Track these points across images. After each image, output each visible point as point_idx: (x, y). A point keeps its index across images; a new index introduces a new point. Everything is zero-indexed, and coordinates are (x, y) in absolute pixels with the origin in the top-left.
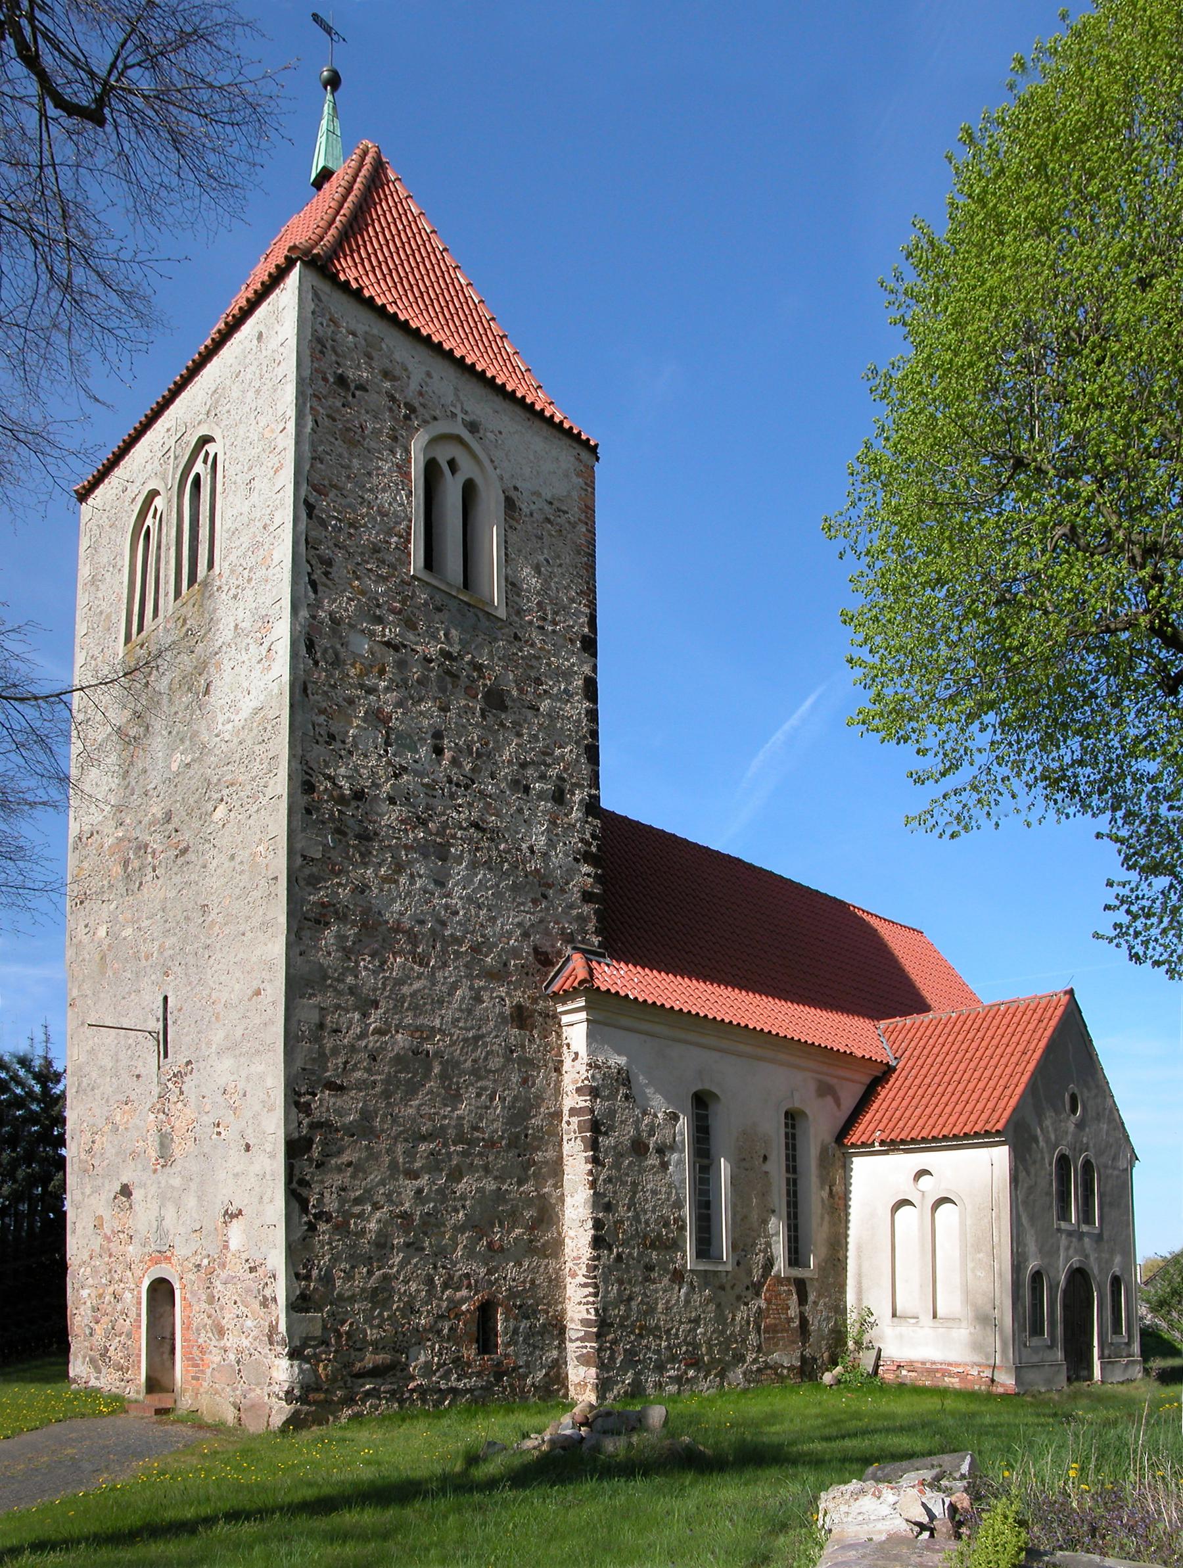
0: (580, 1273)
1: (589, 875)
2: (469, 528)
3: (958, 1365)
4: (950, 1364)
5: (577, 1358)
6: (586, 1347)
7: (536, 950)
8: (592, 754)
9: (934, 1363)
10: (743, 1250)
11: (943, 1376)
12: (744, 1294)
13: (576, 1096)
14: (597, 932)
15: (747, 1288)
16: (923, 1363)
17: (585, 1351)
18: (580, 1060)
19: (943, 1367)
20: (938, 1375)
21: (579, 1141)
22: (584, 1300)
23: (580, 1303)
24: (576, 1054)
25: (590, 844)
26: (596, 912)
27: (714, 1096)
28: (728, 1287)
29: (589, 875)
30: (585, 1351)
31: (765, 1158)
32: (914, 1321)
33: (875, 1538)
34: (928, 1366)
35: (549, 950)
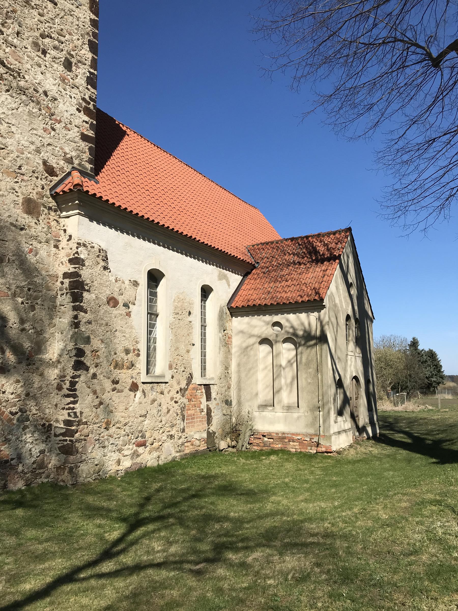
0: (65, 387)
1: (87, 122)
2: (234, 296)
3: (297, 434)
4: (293, 434)
5: (59, 448)
6: (66, 440)
7: (45, 163)
8: (267, 243)
9: (284, 433)
10: (175, 369)
11: (289, 441)
12: (175, 396)
13: (68, 265)
14: (90, 162)
15: (177, 392)
16: (277, 434)
17: (65, 443)
18: (72, 240)
19: (289, 436)
20: (286, 441)
21: (69, 296)
22: (67, 407)
23: (63, 409)
24: (70, 236)
25: (89, 103)
26: (90, 149)
27: (162, 275)
28: (165, 392)
29: (87, 122)
30: (65, 443)
31: (190, 313)
32: (271, 408)
33: (171, 338)
34: (280, 435)
35: (55, 165)
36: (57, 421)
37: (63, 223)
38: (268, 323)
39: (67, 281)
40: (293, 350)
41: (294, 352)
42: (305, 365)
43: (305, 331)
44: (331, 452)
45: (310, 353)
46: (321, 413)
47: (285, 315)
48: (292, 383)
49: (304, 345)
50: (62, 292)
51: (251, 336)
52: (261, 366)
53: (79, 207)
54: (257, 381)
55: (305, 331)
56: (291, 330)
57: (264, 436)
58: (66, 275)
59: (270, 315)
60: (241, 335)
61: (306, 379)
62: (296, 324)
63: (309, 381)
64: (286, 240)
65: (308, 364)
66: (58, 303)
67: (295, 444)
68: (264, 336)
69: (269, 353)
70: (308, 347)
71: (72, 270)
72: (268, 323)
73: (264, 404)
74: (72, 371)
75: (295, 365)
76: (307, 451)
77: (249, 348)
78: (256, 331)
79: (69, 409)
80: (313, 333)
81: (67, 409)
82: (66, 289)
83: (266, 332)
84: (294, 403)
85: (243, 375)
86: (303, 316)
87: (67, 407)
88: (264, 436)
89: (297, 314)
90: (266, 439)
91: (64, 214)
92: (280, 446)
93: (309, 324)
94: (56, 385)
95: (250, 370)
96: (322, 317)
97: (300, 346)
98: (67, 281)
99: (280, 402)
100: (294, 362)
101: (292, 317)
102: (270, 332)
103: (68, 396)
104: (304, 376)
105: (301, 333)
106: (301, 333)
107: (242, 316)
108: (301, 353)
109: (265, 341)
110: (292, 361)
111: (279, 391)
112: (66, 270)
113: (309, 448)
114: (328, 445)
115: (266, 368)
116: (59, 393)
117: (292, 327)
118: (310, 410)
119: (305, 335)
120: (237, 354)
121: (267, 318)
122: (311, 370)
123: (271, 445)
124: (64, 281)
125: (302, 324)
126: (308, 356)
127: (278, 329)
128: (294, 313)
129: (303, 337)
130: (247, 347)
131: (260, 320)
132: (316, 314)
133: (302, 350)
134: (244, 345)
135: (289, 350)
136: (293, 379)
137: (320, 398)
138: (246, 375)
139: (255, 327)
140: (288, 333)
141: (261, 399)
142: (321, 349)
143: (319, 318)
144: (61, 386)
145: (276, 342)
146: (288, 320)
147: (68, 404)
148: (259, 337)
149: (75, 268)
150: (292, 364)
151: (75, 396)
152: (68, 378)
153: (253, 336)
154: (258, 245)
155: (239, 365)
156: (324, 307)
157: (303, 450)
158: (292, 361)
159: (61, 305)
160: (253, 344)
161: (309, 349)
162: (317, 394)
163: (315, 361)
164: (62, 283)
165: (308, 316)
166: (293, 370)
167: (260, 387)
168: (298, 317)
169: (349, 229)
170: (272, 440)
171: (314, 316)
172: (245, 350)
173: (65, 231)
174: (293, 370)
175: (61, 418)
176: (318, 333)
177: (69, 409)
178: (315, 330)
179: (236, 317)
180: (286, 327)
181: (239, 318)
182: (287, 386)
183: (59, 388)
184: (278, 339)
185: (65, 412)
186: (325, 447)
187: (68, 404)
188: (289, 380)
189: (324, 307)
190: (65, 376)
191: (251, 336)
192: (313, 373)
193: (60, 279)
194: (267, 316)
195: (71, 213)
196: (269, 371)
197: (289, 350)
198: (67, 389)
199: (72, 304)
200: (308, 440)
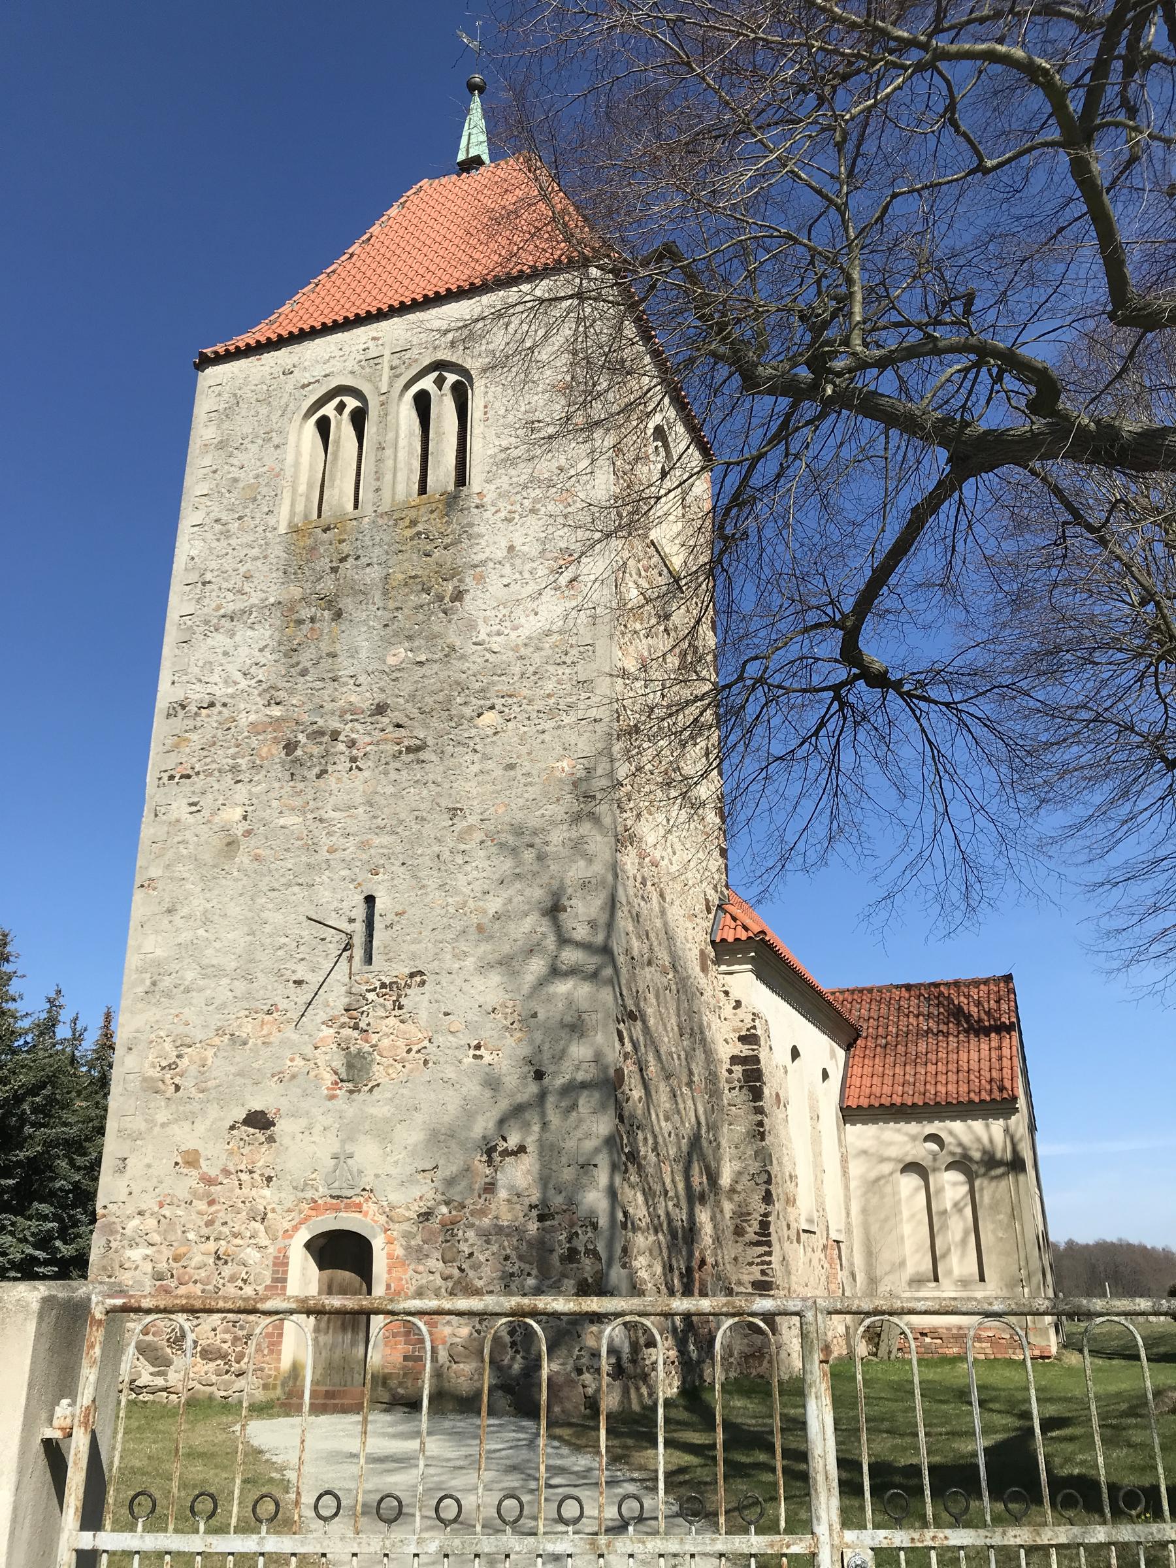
0: (749, 1229)
9: (960, 1328)
13: (739, 1044)
16: (947, 1329)
21: (744, 1091)
22: (759, 1260)
23: (751, 1264)
34: (954, 1331)
36: (740, 1283)
37: (723, 982)
38: (914, 1138)
39: (738, 1069)
40: (962, 1184)
41: (966, 1188)
42: (991, 1208)
43: (984, 1152)
44: (1049, 1357)
45: (997, 1187)
46: (1026, 1290)
47: (948, 1122)
48: (964, 1242)
49: (984, 1175)
50: (732, 1085)
51: (883, 1160)
52: (906, 1214)
53: (752, 961)
54: (902, 1238)
55: (984, 1152)
56: (959, 1150)
57: (923, 1334)
58: (734, 1060)
59: (919, 1121)
60: (863, 1158)
61: (994, 1232)
62: (966, 1139)
63: (1000, 1235)
64: (897, 987)
65: (995, 1207)
66: (726, 1102)
67: (984, 1345)
68: (909, 1159)
69: (917, 1189)
70: (993, 1178)
71: (751, 1053)
72: (914, 1138)
73: (918, 1278)
74: (764, 1206)
75: (968, 1211)
76: (1007, 1356)
77: (882, 1182)
78: (893, 1152)
79: (763, 1263)
80: (999, 1155)
81: (758, 1264)
82: (739, 1081)
83: (914, 1152)
84: (972, 1275)
85: (874, 1228)
86: (978, 1125)
87: (759, 1260)
88: (923, 1334)
89: (969, 1121)
90: (928, 1340)
91: (723, 968)
92: (955, 1350)
93: (991, 1141)
94: (732, 1228)
95: (886, 1220)
96: (1012, 1128)
97: (977, 1177)
98: (738, 1069)
99: (949, 1272)
100: (966, 1205)
101: (957, 1126)
102: (924, 1152)
103: (758, 1244)
104: (990, 1226)
105: (977, 1155)
106: (977, 1155)
107: (864, 1123)
108: (982, 1189)
109: (910, 1166)
110: (962, 1204)
111: (944, 1256)
112: (736, 1052)
113: (1010, 1351)
114: (1044, 1344)
115: (913, 1216)
116: (740, 1239)
117: (960, 1144)
118: (1006, 1285)
119: (986, 1158)
120: (859, 1193)
121: (913, 1128)
122: (1001, 1217)
123: (940, 1351)
124: (734, 1068)
125: (979, 1140)
126: (994, 1192)
127: (934, 1147)
128: (964, 1120)
129: (981, 1162)
130: (878, 1179)
131: (899, 1131)
132: (1001, 1122)
133: (981, 1184)
134: (873, 1175)
135: (955, 1184)
136: (966, 1233)
137: (1022, 1263)
138: (881, 1229)
139: (890, 1144)
140: (953, 1154)
141: (910, 1270)
142: (1017, 1181)
143: (1006, 1130)
144: (743, 1228)
145: (934, 1170)
146: (951, 1133)
147: (759, 1256)
148: (900, 1161)
149: (753, 1050)
150: (960, 1211)
151: (769, 1244)
152: (756, 1216)
153: (888, 1159)
154: (842, 992)
155: (864, 1211)
156: (1016, 1110)
157: (999, 1356)
158: (962, 1204)
159: (730, 1105)
160: (891, 1174)
161: (994, 1184)
162: (1016, 1257)
163: (1007, 1200)
164: (730, 1071)
165: (987, 1126)
166: (964, 1219)
167: (909, 1246)
168: (969, 1127)
169: (1008, 978)
170: (939, 1341)
171: (997, 1127)
172: (874, 1185)
173: (727, 993)
174: (964, 1219)
175: (746, 1278)
176: (1009, 1155)
177: (763, 1263)
178: (1002, 1149)
179: (853, 1123)
180: (950, 1144)
181: (859, 1125)
182: (956, 1246)
183: (739, 1232)
184: (938, 1164)
185: (756, 1270)
186: (1041, 1348)
187: (759, 1256)
188: (958, 1236)
189: (1016, 1110)
190: (749, 1214)
191: (883, 1160)
192: (1006, 1221)
193: (727, 1066)
194: (914, 1123)
195: (736, 967)
196: (920, 1222)
197: (955, 1184)
198: (755, 1233)
199: (752, 1104)
200: (1008, 1336)
